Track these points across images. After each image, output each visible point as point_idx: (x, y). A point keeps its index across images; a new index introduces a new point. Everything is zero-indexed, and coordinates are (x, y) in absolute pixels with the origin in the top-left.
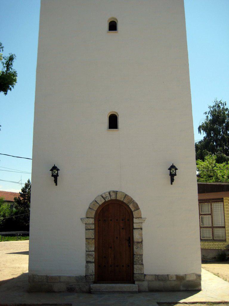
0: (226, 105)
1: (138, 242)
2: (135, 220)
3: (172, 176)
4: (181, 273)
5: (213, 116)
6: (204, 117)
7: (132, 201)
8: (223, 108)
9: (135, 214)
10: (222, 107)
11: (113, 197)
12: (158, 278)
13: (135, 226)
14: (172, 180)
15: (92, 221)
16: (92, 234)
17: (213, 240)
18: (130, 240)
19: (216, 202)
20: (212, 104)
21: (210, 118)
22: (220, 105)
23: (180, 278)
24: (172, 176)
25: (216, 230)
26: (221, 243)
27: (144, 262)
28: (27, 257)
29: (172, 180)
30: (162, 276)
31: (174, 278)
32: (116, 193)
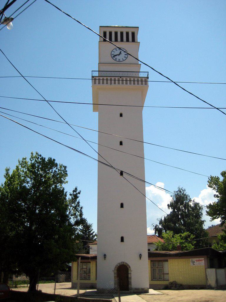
0: (185, 190)
1: (130, 278)
2: (129, 271)
3: (140, 257)
4: (143, 287)
5: (177, 198)
6: (171, 198)
7: (128, 265)
8: (183, 193)
9: (129, 269)
10: (182, 192)
11: (122, 264)
12: (136, 289)
13: (129, 273)
14: (140, 259)
15: (116, 271)
16: (116, 275)
17: (164, 280)
18: (128, 277)
19: (165, 261)
20: (177, 190)
21: (175, 199)
22: (181, 191)
23: (143, 289)
24: (140, 257)
25: (165, 275)
26: (167, 282)
27: (132, 284)
28: (207, 269)
29: (140, 259)
30: (137, 288)
31: (141, 289)
32: (123, 262)
